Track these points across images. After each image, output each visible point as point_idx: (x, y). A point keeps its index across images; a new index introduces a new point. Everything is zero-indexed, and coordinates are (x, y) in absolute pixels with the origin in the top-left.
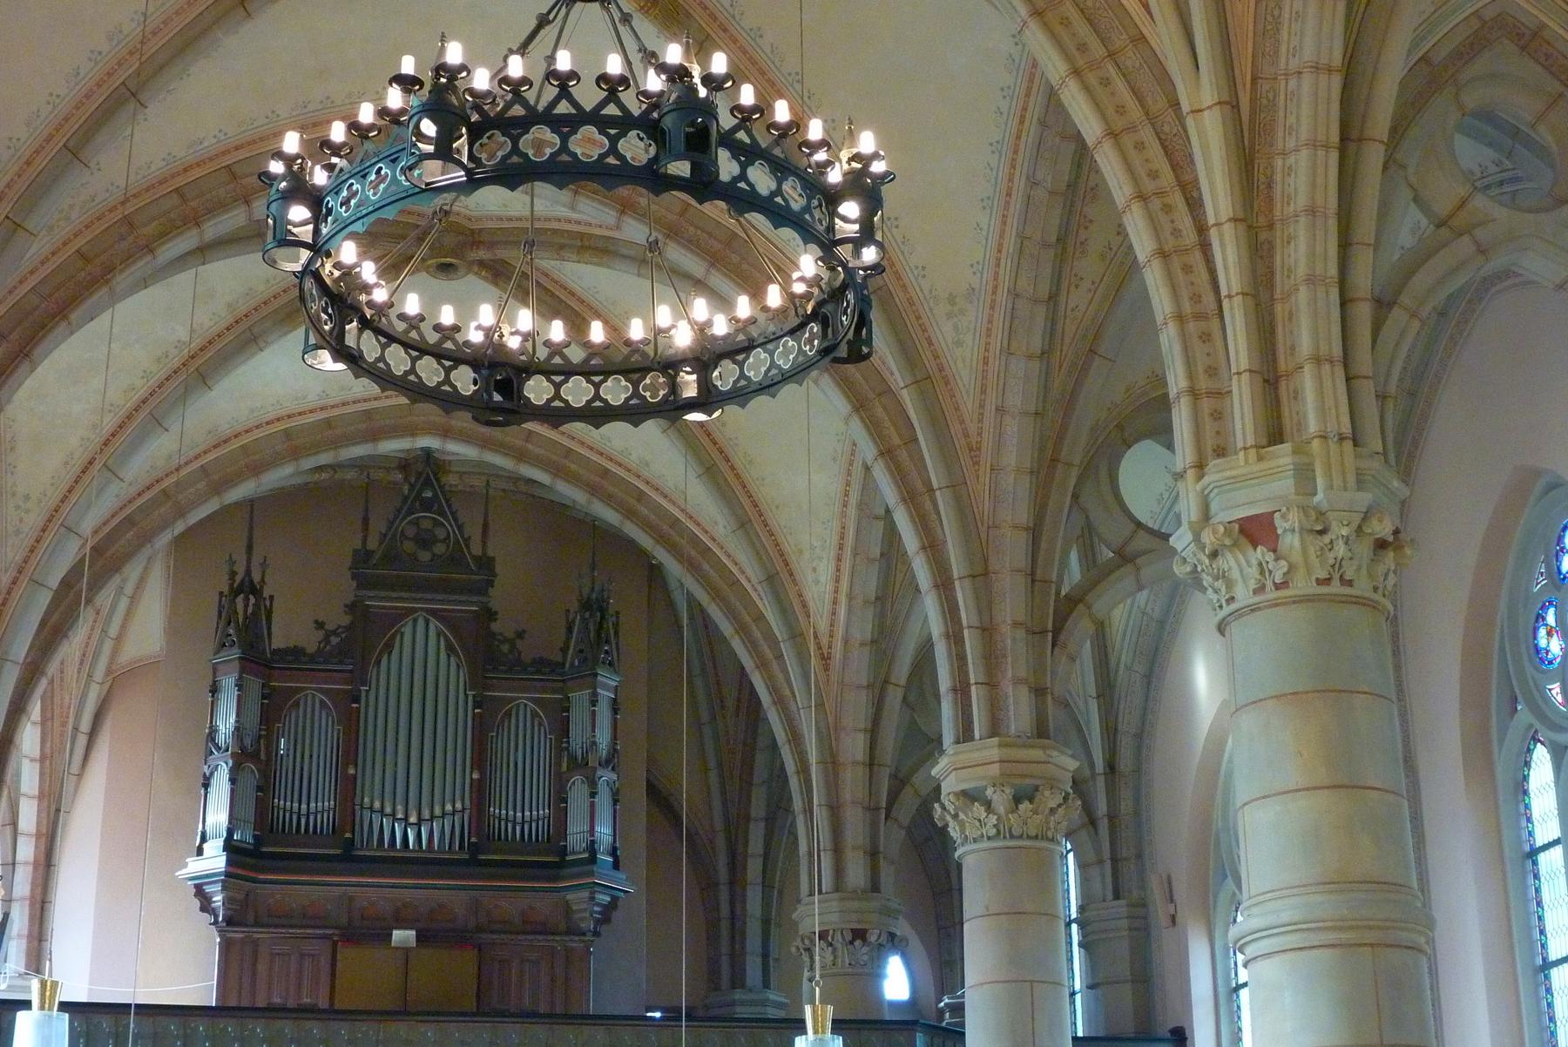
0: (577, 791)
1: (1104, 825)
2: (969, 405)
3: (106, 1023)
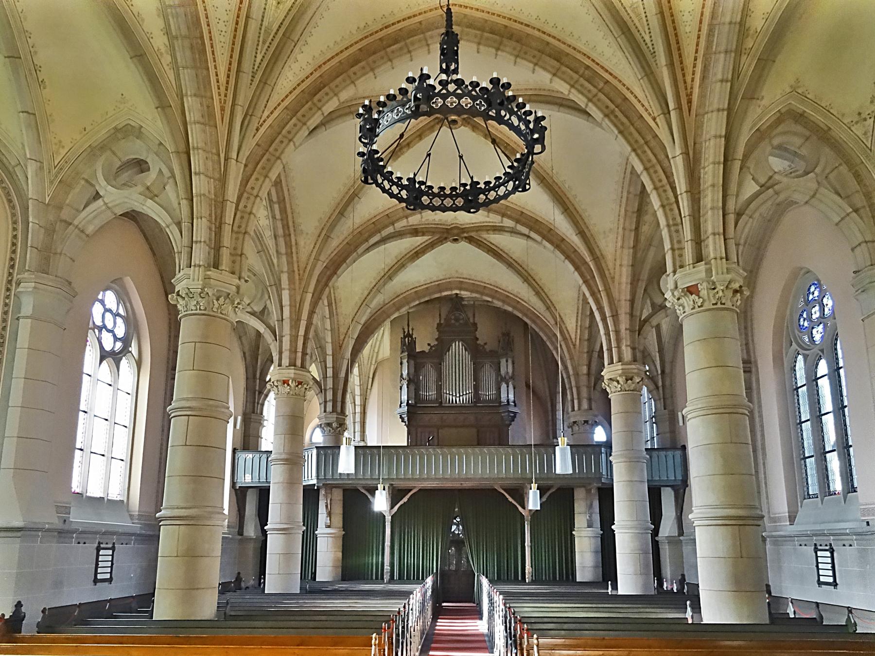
0: (504, 386)
1: (661, 389)
2: (611, 265)
3: (375, 451)
